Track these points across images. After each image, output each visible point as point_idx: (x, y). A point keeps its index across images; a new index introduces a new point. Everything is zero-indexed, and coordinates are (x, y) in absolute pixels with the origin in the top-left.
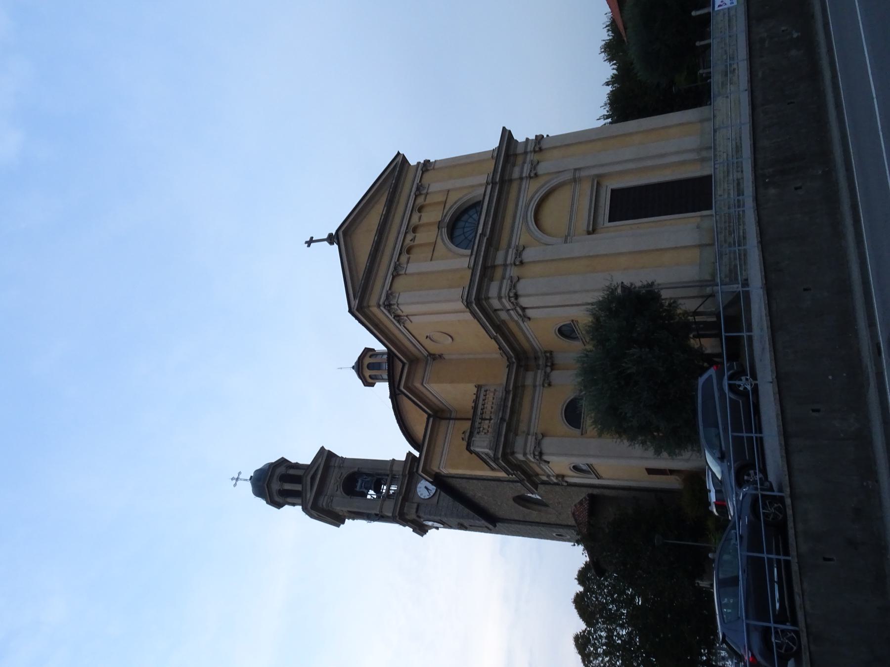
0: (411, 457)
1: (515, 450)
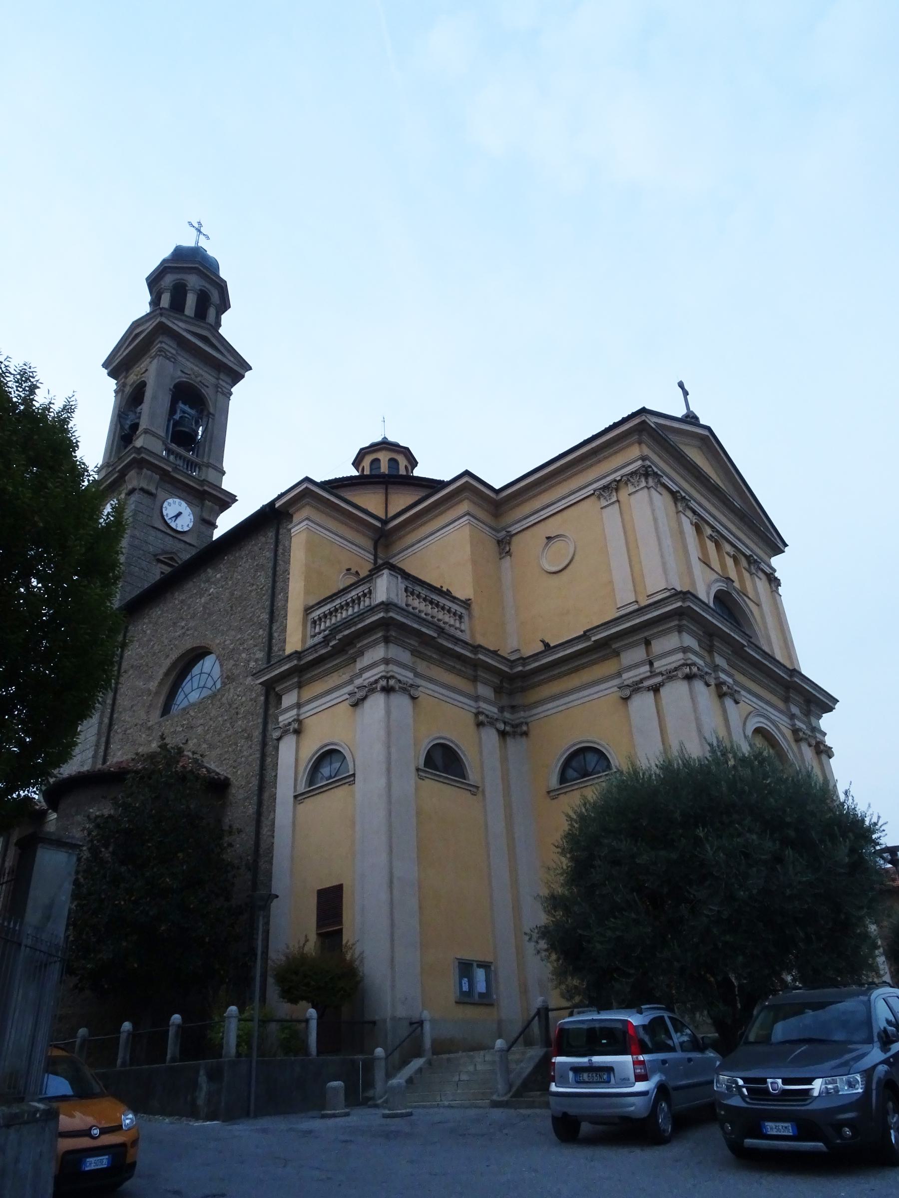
0: (229, 501)
1: (391, 645)
